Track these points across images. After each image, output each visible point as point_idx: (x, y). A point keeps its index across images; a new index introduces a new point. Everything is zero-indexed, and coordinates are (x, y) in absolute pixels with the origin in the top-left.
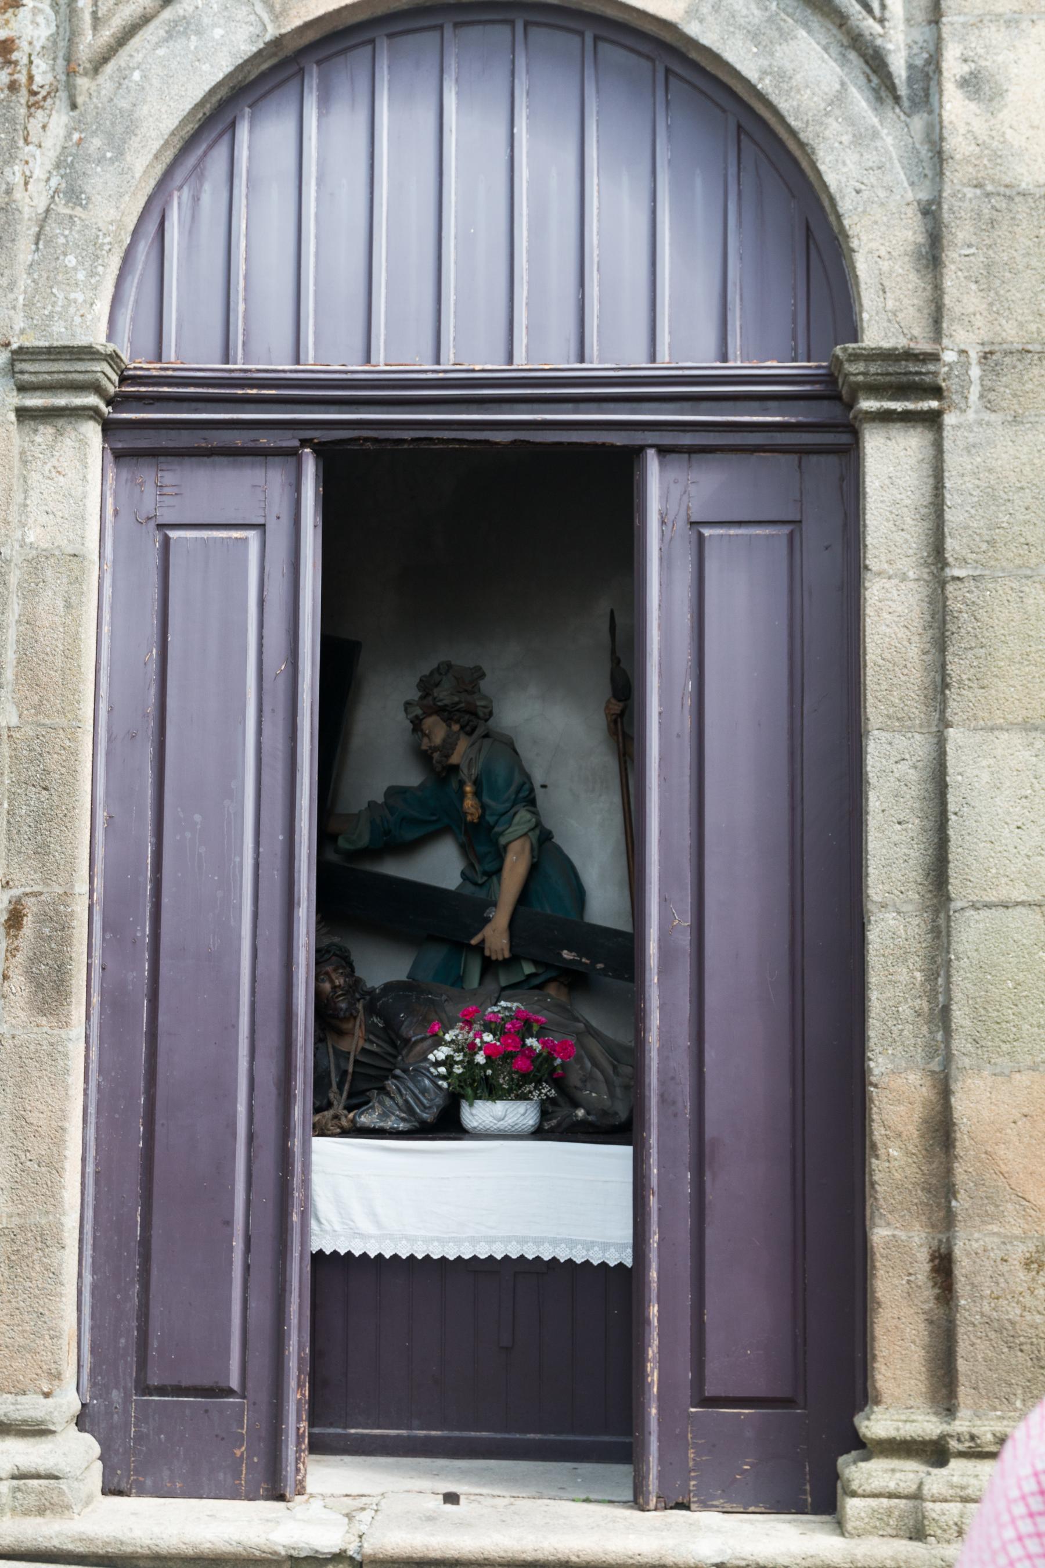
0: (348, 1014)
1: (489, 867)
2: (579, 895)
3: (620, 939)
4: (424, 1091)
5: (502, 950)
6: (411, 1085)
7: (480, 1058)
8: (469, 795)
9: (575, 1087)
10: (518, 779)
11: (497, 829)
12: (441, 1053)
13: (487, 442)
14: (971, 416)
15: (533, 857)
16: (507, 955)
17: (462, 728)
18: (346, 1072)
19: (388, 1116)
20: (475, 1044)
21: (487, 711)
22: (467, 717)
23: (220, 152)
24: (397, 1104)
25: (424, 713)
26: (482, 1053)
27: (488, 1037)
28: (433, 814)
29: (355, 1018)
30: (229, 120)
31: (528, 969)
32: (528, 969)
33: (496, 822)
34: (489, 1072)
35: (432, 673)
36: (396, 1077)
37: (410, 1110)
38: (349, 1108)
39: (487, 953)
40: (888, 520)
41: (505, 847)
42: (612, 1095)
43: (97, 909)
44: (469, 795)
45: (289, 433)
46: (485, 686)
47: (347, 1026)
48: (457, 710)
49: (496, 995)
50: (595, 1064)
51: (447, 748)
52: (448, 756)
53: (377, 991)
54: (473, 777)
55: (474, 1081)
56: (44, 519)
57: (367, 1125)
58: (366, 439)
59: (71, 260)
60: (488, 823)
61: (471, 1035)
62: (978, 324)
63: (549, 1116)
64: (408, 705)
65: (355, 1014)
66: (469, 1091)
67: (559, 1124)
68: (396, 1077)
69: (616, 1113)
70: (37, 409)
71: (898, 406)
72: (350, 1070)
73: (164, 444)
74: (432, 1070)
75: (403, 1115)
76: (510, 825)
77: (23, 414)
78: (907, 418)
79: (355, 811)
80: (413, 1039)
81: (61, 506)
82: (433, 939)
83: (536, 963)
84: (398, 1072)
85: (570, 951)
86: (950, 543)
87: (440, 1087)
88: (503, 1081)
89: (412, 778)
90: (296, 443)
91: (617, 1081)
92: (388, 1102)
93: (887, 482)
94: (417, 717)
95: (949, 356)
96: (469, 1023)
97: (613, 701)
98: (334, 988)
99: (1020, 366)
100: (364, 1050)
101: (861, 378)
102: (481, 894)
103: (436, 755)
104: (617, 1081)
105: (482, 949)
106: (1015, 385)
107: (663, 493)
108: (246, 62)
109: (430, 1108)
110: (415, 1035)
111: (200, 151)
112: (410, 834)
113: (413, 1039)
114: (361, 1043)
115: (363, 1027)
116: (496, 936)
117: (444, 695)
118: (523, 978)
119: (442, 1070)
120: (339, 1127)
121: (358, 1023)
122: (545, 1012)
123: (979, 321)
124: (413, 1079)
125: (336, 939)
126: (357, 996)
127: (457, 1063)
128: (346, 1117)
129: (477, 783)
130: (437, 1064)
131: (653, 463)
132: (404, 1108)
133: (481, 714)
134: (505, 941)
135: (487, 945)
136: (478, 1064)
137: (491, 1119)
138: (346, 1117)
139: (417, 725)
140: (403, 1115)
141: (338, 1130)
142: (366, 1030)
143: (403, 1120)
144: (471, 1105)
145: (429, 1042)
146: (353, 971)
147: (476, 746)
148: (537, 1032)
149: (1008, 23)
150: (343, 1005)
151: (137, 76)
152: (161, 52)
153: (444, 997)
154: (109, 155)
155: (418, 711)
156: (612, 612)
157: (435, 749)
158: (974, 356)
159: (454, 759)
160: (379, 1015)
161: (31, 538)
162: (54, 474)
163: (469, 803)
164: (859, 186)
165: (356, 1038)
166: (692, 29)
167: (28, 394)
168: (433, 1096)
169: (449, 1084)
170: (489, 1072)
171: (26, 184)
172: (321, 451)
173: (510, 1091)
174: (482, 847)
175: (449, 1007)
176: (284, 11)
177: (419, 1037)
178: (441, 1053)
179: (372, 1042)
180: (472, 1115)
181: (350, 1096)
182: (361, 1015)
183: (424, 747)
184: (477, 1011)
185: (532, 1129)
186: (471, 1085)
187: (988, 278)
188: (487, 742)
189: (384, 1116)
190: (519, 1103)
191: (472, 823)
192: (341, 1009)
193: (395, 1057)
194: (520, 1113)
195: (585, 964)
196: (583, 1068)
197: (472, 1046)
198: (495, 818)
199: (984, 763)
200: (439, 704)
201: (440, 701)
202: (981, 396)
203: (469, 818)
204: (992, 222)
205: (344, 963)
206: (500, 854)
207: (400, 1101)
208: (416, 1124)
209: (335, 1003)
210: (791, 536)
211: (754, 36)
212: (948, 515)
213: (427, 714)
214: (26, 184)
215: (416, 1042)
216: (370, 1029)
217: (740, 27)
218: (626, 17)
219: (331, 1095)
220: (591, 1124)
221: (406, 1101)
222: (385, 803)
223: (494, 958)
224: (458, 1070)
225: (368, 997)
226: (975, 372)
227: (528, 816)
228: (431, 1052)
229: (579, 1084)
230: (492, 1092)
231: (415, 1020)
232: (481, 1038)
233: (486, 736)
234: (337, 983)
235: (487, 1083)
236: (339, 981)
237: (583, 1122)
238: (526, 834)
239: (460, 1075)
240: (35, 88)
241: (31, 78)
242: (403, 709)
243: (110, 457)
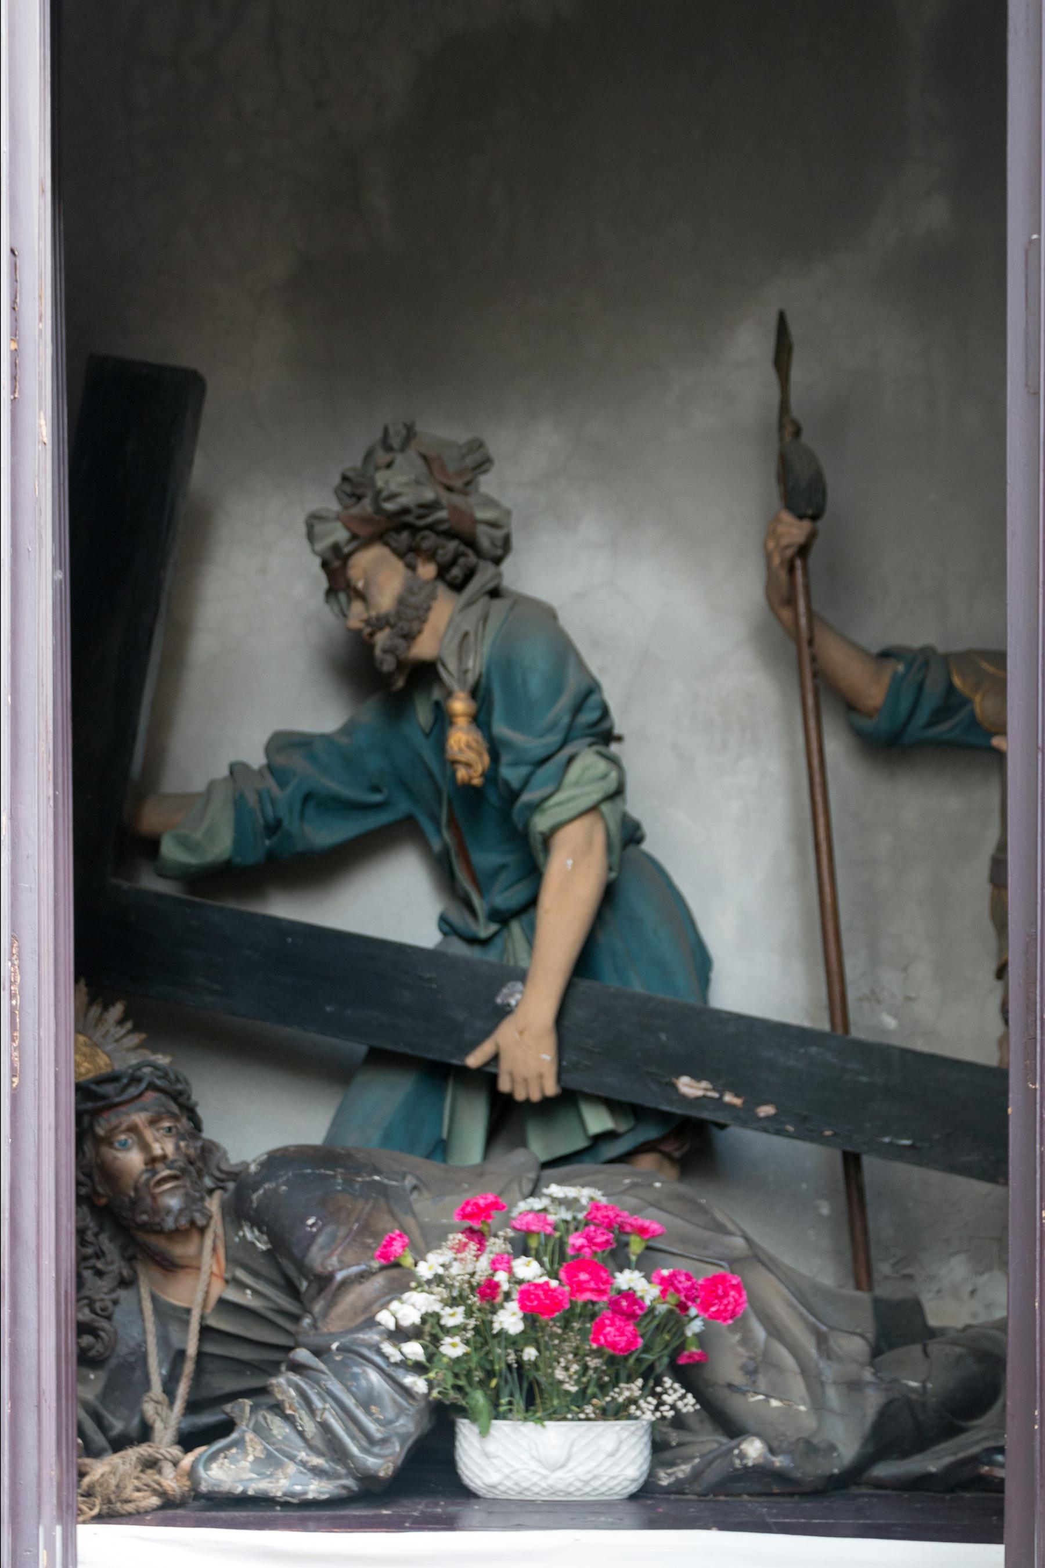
0: (183, 1222)
1: (505, 898)
2: (701, 963)
3: (813, 1050)
4: (368, 1401)
5: (541, 1076)
6: (335, 1386)
7: (510, 1319)
8: (462, 722)
9: (730, 1386)
10: (573, 685)
11: (527, 797)
12: (409, 1309)
15: (610, 869)
16: (551, 1089)
17: (442, 573)
18: (181, 1354)
19: (279, 1465)
20: (497, 1285)
21: (499, 534)
22: (452, 545)
24: (301, 1434)
25: (354, 537)
26: (513, 1306)
27: (528, 1269)
28: (376, 789)
29: (202, 1231)
31: (598, 1121)
32: (598, 1121)
33: (526, 782)
34: (530, 1353)
36: (297, 1368)
37: (335, 1450)
38: (188, 1441)
39: (504, 1085)
41: (547, 840)
42: (818, 1405)
44: (462, 722)
47: (181, 1250)
48: (430, 527)
49: (532, 1175)
50: (775, 1331)
51: (408, 619)
52: (410, 637)
53: (253, 1168)
54: (471, 678)
55: (490, 1374)
57: (225, 1487)
60: (506, 783)
61: (483, 1264)
63: (667, 1455)
64: (313, 521)
65: (200, 1221)
66: (479, 1398)
67: (696, 1475)
68: (297, 1368)
69: (833, 1448)
72: (192, 1349)
74: (387, 1348)
75: (317, 1461)
76: (558, 789)
79: (199, 785)
80: (340, 1276)
82: (381, 1059)
83: (613, 1106)
84: (302, 1355)
85: (697, 1077)
87: (407, 1392)
88: (565, 1375)
91: (829, 1371)
92: (279, 1428)
94: (336, 548)
96: (479, 1237)
97: (787, 517)
98: (152, 1161)
100: (223, 1304)
103: (382, 638)
104: (829, 1371)
105: (493, 1078)
109: (384, 1441)
110: (344, 1265)
112: (324, 833)
113: (340, 1276)
114: (218, 1289)
115: (221, 1252)
116: (525, 1049)
118: (581, 1143)
119: (414, 1350)
120: (155, 1492)
121: (208, 1242)
122: (652, 1211)
124: (340, 1372)
125: (162, 1060)
126: (208, 1182)
127: (448, 1331)
128: (175, 1464)
129: (479, 693)
130: (400, 1335)
132: (318, 1443)
133: (485, 543)
135: (505, 1066)
136: (502, 1333)
137: (534, 1466)
138: (175, 1464)
139: (335, 569)
140: (317, 1461)
141: (155, 1501)
142: (228, 1259)
143: (318, 1472)
144: (484, 1432)
145: (378, 1282)
146: (197, 1126)
147: (477, 609)
148: (640, 1257)
150: (174, 1202)
153: (409, 1181)
155: (341, 534)
156: (782, 318)
157: (379, 623)
159: (424, 648)
160: (256, 1222)
163: (462, 739)
165: (204, 1277)
168: (390, 1414)
169: (431, 1385)
170: (530, 1353)
173: (581, 1398)
174: (487, 839)
175: (423, 1204)
177: (354, 1270)
178: (409, 1309)
180: (487, 1455)
181: (193, 1407)
182: (216, 1226)
184: (496, 1206)
185: (633, 1488)
186: (483, 1384)
188: (497, 604)
189: (270, 1461)
190: (601, 1425)
192: (169, 1211)
193: (296, 1319)
194: (608, 1453)
195: (731, 1106)
196: (747, 1340)
197: (489, 1290)
198: (524, 770)
200: (389, 506)
201: (392, 497)
203: (462, 773)
205: (175, 1108)
206: (530, 864)
207: (310, 1428)
208: (350, 1482)
209: (154, 1198)
213: (361, 541)
215: (346, 1283)
216: (238, 1257)
219: (149, 1408)
220: (780, 1476)
221: (325, 1427)
222: (270, 767)
223: (520, 1096)
224: (453, 1348)
225: (231, 1186)
227: (602, 766)
228: (385, 1306)
229: (738, 1378)
230: (531, 1395)
231: (342, 1232)
232: (510, 1270)
233: (495, 593)
234: (157, 1150)
235: (521, 1377)
236: (163, 1146)
237: (761, 1473)
238: (594, 809)
239: (457, 1360)
242: (302, 529)
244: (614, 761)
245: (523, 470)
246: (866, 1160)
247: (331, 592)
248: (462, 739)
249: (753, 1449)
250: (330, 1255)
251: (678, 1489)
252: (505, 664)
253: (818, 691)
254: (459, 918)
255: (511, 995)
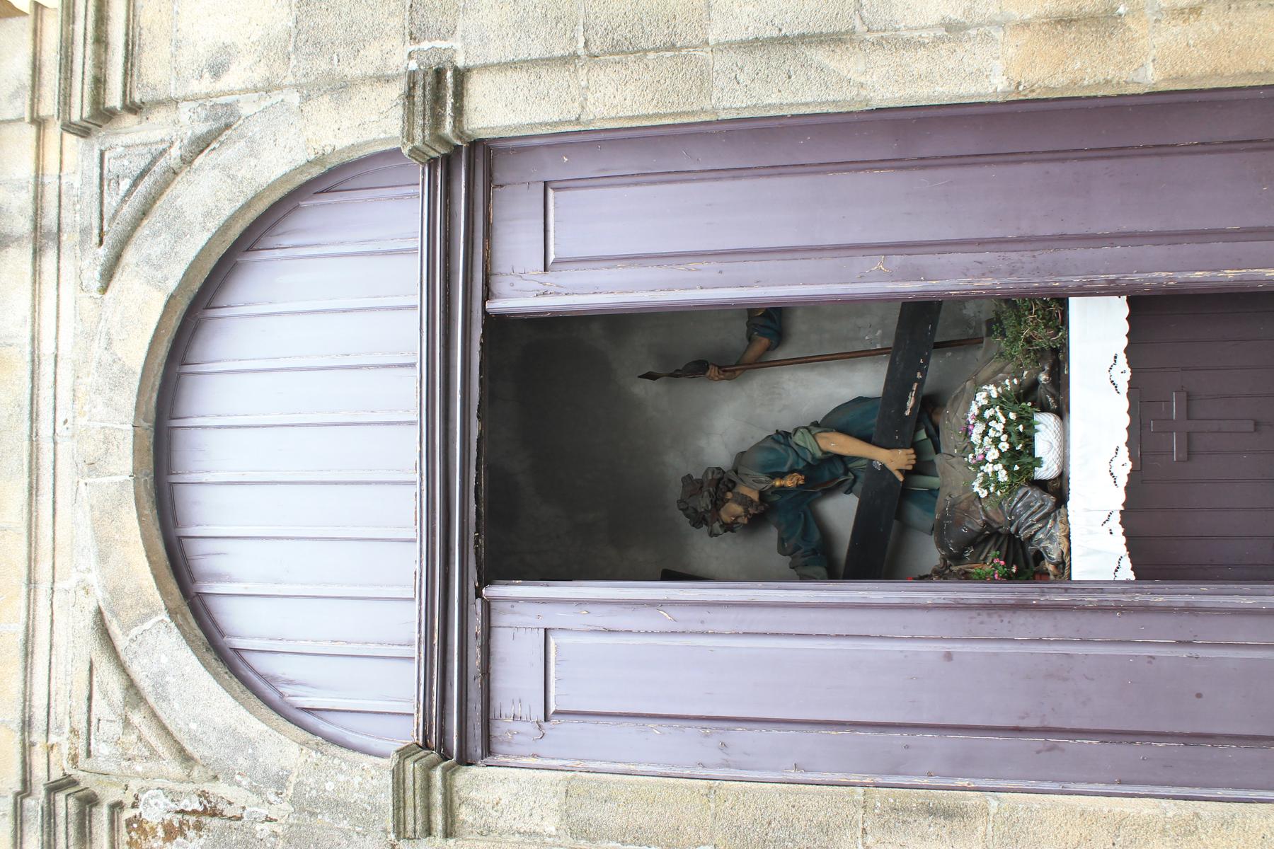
2: (860, 400)
10: (770, 444)
11: (810, 460)
13: (479, 441)
14: (458, 45)
17: (730, 490)
23: (254, 660)
30: (231, 653)
31: (922, 435)
32: (922, 435)
35: (688, 516)
36: (1017, 530)
39: (910, 468)
40: (540, 105)
41: (825, 453)
43: (879, 780)
45: (471, 607)
46: (697, 475)
51: (745, 501)
52: (752, 501)
56: (536, 819)
58: (476, 542)
59: (330, 786)
62: (389, 47)
67: (1053, 396)
68: (1017, 530)
70: (446, 820)
71: (450, 101)
73: (478, 714)
77: (448, 834)
78: (459, 94)
81: (526, 803)
82: (900, 514)
83: (917, 430)
84: (1013, 529)
86: (558, 52)
89: (771, 536)
90: (479, 600)
93: (510, 107)
95: (413, 65)
99: (421, 12)
101: (427, 132)
102: (862, 476)
103: (752, 511)
106: (437, 13)
107: (521, 294)
108: (185, 637)
111: (251, 674)
116: (896, 460)
117: (704, 503)
123: (387, 47)
129: (774, 476)
131: (495, 306)
134: (900, 451)
135: (904, 468)
139: (728, 528)
149: (178, 47)
151: (193, 726)
152: (177, 706)
154: (250, 751)
157: (746, 511)
158: (414, 47)
159: (755, 496)
160: (963, 551)
161: (552, 830)
162: (499, 808)
163: (789, 482)
164: (287, 150)
166: (172, 285)
167: (433, 826)
171: (271, 820)
172: (488, 577)
174: (827, 474)
176: (148, 605)
179: (986, 557)
183: (746, 521)
187: (355, 46)
191: (805, 480)
194: (1046, 424)
199: (737, 10)
202: (444, 39)
204: (315, 44)
210: (555, 189)
211: (179, 237)
212: (535, 55)
214: (271, 820)
215: (987, 516)
217: (172, 249)
218: (166, 339)
220: (1052, 368)
221: (1038, 521)
226: (425, 45)
227: (798, 434)
233: (736, 472)
237: (1050, 374)
238: (814, 436)
240: (201, 809)
241: (194, 812)
243: (489, 760)
244: (796, 430)
245: (677, 466)
246: (937, 340)
247: (732, 531)
248: (789, 482)
249: (1043, 377)
250: (977, 523)
251: (1057, 402)
252: (764, 468)
253: (761, 363)
254: (846, 487)
255: (877, 465)
